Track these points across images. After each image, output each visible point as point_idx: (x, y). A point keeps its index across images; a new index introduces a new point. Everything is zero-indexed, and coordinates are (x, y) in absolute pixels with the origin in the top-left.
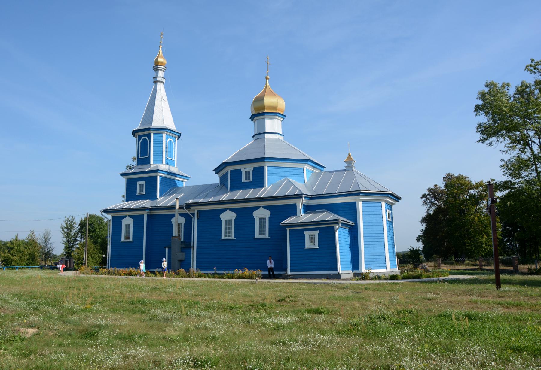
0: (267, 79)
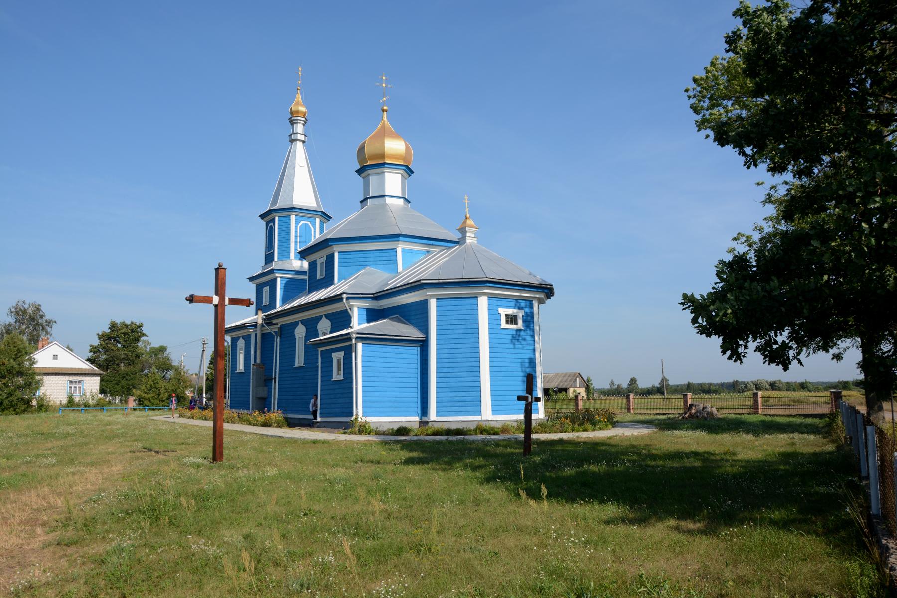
0: (383, 110)
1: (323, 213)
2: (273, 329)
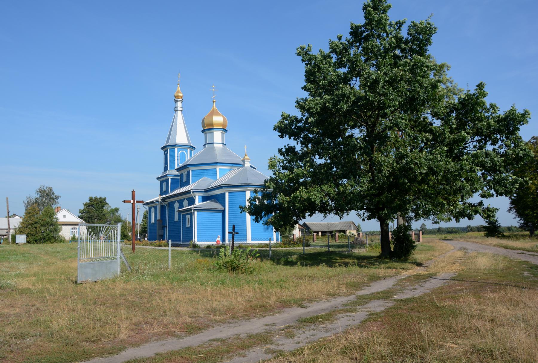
1: (191, 146)
2: (165, 204)
